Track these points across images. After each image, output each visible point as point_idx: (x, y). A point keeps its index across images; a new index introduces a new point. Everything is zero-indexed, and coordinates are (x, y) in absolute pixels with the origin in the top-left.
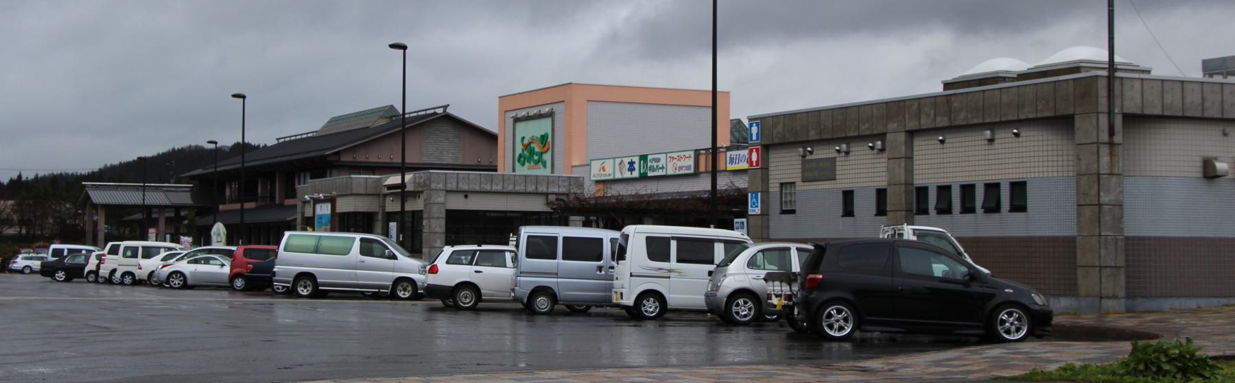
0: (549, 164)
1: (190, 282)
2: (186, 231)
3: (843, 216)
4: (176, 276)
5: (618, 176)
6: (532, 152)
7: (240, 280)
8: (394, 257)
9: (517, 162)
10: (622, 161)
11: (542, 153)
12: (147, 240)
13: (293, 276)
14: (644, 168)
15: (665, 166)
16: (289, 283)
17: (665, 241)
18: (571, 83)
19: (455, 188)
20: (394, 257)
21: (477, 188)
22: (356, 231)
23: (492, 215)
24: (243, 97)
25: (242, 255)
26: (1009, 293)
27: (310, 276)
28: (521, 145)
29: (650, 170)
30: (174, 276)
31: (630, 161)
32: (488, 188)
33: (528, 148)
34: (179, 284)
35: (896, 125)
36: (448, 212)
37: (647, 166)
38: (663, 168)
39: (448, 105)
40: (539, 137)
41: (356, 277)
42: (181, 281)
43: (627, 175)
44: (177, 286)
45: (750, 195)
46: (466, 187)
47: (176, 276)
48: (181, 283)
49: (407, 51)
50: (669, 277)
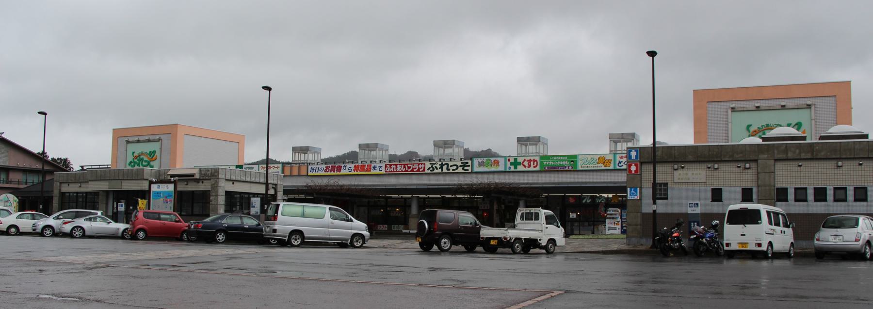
1: (87, 233)
2: (597, 199)
3: (711, 201)
4: (77, 229)
7: (139, 233)
8: (352, 221)
11: (150, 161)
13: (289, 232)
16: (286, 237)
17: (776, 214)
18: (177, 124)
19: (229, 179)
20: (352, 221)
21: (239, 179)
22: (326, 203)
24: (45, 114)
25: (143, 217)
26: (457, 240)
27: (300, 233)
30: (76, 229)
32: (243, 179)
33: (138, 158)
34: (79, 235)
35: (766, 156)
36: (226, 192)
39: (751, 125)
40: (148, 152)
41: (329, 233)
42: (81, 232)
44: (78, 236)
45: (629, 189)
46: (233, 178)
47: (77, 229)
48: (81, 234)
49: (271, 91)
50: (773, 234)
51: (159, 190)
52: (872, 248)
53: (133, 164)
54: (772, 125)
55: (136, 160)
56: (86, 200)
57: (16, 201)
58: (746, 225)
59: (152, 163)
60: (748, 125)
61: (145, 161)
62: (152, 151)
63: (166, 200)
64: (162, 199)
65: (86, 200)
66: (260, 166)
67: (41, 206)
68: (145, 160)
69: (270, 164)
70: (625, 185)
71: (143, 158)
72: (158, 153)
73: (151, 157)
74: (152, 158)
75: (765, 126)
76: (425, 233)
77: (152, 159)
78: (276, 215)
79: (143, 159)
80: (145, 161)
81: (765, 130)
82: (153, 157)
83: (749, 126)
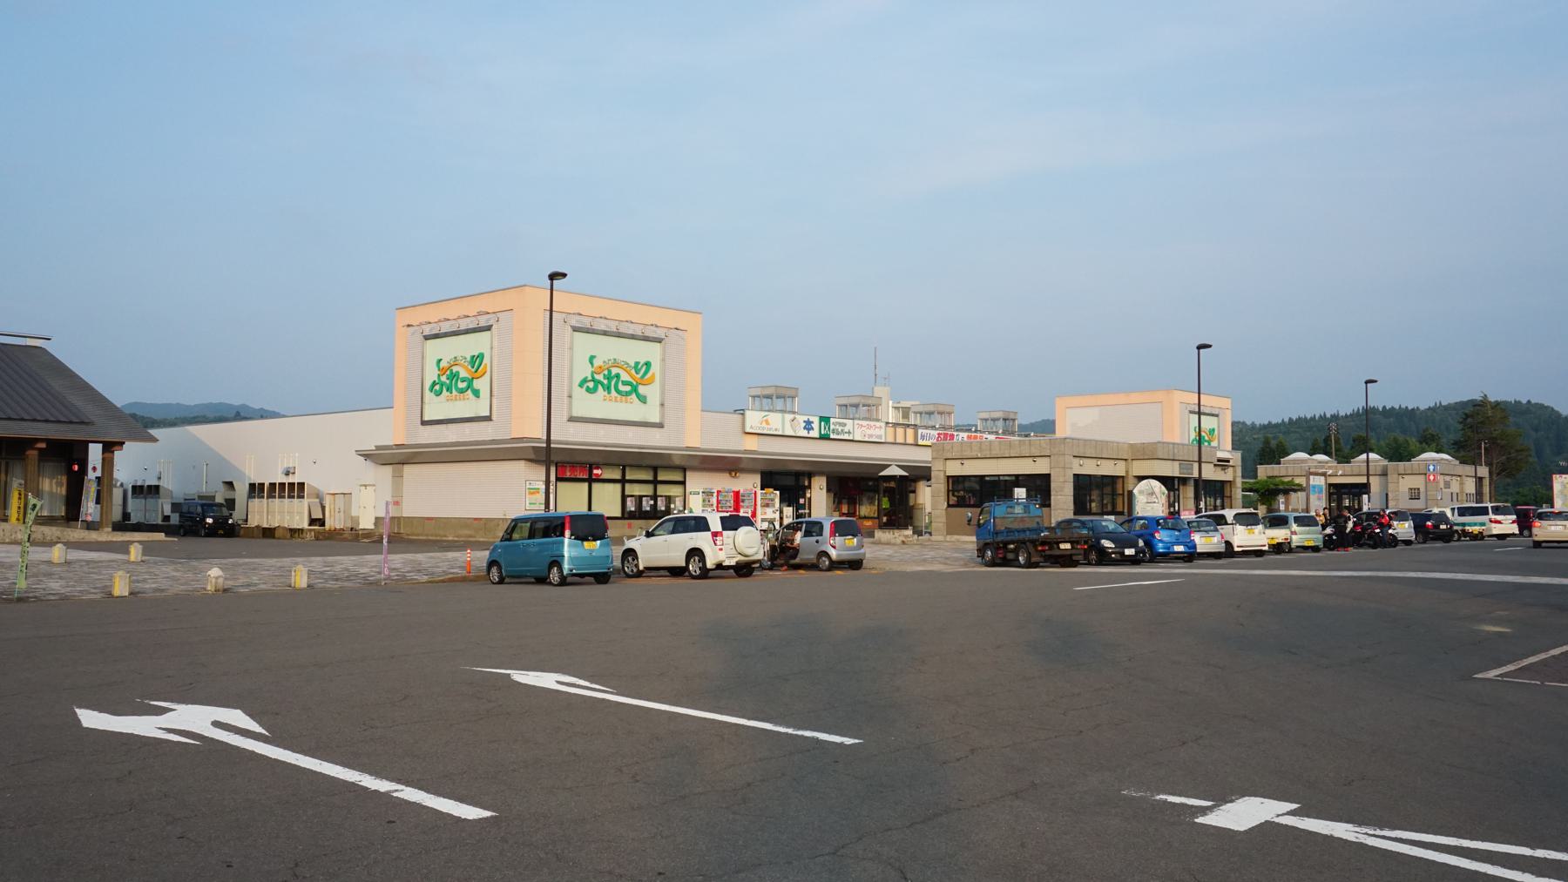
0: (485, 393)
5: (789, 432)
6: (454, 376)
9: (427, 393)
10: (795, 418)
11: (473, 378)
12: (132, 498)
14: (825, 428)
15: (851, 431)
23: (1007, 478)
28: (437, 369)
29: (833, 433)
31: (806, 419)
33: (448, 372)
37: (829, 428)
38: (849, 432)
43: (804, 433)
53: (437, 387)
55: (444, 378)
57: (1164, 494)
59: (642, 390)
61: (626, 383)
62: (476, 354)
66: (856, 422)
67: (989, 553)
68: (622, 379)
71: (458, 372)
72: (656, 369)
73: (473, 370)
76: (494, 814)
79: (618, 376)
80: (626, 383)
82: (478, 368)
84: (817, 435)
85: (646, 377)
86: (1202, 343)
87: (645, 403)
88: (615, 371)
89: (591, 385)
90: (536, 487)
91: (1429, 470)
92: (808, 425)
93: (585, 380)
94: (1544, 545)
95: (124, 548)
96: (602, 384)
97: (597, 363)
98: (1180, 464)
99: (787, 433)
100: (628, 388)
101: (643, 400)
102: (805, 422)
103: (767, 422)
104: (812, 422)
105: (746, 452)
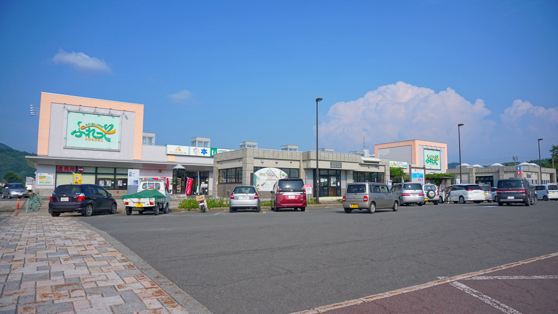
43: (202, 155)
51: (415, 173)
52: (376, 205)
54: (95, 124)
56: (227, 175)
58: (357, 193)
59: (437, 162)
60: (79, 122)
63: (420, 179)
64: (418, 178)
65: (227, 175)
69: (464, 163)
70: (213, 166)
74: (109, 131)
75: (91, 124)
77: (108, 133)
78: (125, 184)
79: (432, 159)
81: (90, 126)
83: (80, 122)
84: (209, 156)
85: (110, 131)
86: (318, 98)
87: (110, 142)
88: (92, 128)
89: (428, 161)
90: (44, 175)
91: (518, 169)
92: (204, 151)
93: (75, 132)
94: (239, 210)
95: (153, 199)
96: (429, 161)
97: (429, 156)
98: (331, 163)
99: (191, 154)
100: (434, 162)
101: (109, 140)
102: (202, 150)
103: (180, 150)
104: (207, 150)
105: (168, 162)
